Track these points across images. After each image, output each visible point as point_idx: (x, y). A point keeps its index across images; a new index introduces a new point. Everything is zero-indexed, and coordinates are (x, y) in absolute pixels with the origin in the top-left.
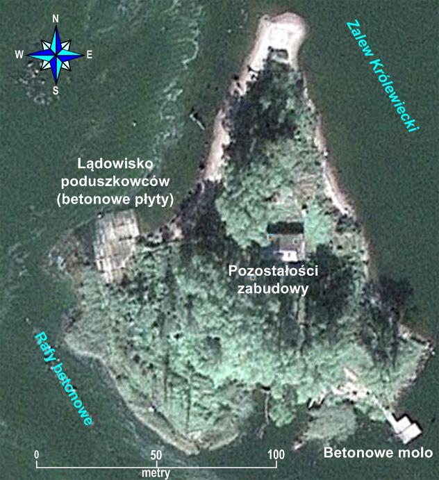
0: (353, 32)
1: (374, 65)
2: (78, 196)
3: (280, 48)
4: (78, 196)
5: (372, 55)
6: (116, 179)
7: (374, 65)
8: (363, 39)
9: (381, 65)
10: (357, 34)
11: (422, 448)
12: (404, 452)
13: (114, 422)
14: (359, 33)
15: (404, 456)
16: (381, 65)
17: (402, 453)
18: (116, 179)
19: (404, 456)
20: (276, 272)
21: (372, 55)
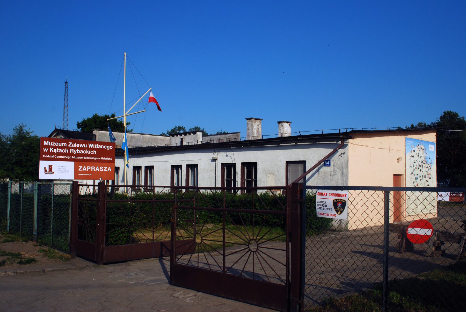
0: (73, 146)
1: (51, 151)
2: (56, 149)
3: (349, 155)
4: (56, 149)
5: (47, 149)
6: (88, 151)
7: (51, 151)
8: (76, 144)
9: (53, 148)
10: (74, 145)
11: (76, 143)
12: (64, 144)
13: (306, 203)
14: (74, 144)
15: (64, 146)
16: (53, 148)
17: (63, 144)
18: (88, 151)
19: (64, 146)
20: (59, 150)
21: (47, 149)
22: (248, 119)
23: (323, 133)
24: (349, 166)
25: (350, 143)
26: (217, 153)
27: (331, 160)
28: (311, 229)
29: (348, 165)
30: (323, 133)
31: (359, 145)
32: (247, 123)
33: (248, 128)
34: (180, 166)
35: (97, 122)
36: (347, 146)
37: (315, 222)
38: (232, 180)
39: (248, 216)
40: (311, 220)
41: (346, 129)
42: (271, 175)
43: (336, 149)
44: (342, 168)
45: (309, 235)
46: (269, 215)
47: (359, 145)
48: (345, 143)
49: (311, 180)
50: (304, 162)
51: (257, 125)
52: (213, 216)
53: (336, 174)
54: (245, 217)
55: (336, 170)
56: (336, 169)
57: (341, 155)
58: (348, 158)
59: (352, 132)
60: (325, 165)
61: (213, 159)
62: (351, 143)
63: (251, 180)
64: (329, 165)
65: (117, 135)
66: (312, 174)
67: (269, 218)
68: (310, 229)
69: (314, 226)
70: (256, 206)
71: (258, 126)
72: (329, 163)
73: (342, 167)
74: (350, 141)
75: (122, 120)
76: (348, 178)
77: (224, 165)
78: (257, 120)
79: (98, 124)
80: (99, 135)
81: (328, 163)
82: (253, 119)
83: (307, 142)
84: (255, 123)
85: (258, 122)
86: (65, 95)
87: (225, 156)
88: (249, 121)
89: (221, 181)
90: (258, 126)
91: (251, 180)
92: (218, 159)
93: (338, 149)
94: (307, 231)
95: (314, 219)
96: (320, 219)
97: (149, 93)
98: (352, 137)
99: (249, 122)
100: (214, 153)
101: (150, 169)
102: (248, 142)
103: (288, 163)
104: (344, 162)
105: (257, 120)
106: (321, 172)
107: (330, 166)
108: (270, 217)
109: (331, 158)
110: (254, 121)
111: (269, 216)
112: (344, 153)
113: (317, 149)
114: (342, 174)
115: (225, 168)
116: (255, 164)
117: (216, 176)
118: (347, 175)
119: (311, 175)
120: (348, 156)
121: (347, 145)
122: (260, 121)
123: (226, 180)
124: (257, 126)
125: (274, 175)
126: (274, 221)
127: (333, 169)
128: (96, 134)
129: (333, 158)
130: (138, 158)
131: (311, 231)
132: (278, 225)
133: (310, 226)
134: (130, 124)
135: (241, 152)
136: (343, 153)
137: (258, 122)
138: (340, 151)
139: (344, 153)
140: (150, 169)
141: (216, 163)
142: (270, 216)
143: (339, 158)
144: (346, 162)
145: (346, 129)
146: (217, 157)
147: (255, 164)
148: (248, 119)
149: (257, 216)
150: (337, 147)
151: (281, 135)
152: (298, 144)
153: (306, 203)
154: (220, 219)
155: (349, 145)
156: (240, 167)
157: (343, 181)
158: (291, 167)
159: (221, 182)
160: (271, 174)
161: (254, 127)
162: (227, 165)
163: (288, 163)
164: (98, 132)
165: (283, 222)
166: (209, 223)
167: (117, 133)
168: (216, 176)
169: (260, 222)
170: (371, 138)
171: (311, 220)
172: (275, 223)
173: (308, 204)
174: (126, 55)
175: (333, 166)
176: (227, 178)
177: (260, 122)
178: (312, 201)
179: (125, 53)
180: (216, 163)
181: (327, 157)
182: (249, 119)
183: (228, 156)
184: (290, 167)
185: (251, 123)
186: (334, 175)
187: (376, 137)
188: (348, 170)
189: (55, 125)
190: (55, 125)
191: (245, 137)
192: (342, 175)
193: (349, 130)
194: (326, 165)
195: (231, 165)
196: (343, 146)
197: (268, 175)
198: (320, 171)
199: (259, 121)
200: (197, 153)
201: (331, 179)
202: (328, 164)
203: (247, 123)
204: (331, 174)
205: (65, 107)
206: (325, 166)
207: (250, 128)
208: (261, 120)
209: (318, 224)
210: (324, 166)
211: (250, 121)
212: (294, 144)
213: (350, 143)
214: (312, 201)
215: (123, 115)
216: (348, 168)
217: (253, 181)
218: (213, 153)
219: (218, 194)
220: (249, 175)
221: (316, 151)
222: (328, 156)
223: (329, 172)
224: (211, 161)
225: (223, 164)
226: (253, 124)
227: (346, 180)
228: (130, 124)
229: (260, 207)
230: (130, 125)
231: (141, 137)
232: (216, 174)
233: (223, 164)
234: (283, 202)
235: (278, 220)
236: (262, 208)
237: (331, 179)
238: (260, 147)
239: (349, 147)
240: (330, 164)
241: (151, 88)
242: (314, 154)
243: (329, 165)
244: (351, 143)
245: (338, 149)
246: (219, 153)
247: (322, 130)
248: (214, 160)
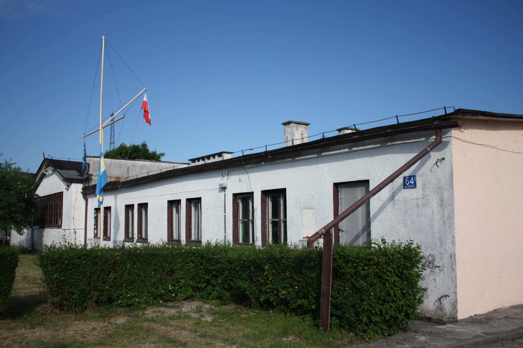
3: (453, 162)
22: (285, 124)
23: (400, 122)
24: (454, 185)
25: (455, 137)
26: (226, 178)
27: (417, 175)
28: (372, 325)
29: (452, 182)
30: (398, 122)
31: (474, 143)
32: (285, 130)
33: (286, 138)
34: (179, 201)
35: (123, 154)
36: (448, 144)
37: (381, 311)
38: (250, 222)
39: (254, 291)
40: (371, 306)
41: (445, 108)
42: (309, 210)
43: (426, 149)
44: (440, 190)
45: (367, 339)
46: (289, 290)
47: (474, 143)
48: (443, 138)
49: (380, 217)
50: (367, 182)
51: (300, 133)
52: (203, 286)
53: (428, 203)
54: (247, 292)
55: (428, 195)
56: (427, 193)
57: (436, 163)
58: (452, 169)
59: (458, 112)
60: (406, 187)
61: (221, 187)
62: (458, 139)
63: (278, 220)
64: (414, 186)
65: (120, 164)
66: (382, 206)
67: (289, 296)
68: (370, 325)
69: (378, 319)
70: (265, 271)
71: (302, 134)
72: (413, 182)
73: (440, 188)
74: (455, 133)
75: (155, 151)
76: (453, 211)
77: (238, 197)
78: (301, 126)
79: (124, 155)
80: (94, 164)
81: (411, 182)
82: (292, 123)
83: (369, 145)
84: (297, 129)
85: (302, 128)
86: (111, 130)
87: (238, 181)
88: (287, 126)
89: (232, 223)
90: (302, 134)
91: (278, 220)
92: (228, 187)
93: (429, 149)
94: (363, 328)
95: (378, 302)
96: (392, 302)
97: (142, 95)
98: (459, 123)
99: (288, 128)
100: (222, 178)
101: (143, 206)
102: (269, 153)
103: (337, 186)
104: (445, 177)
105: (300, 125)
106: (398, 200)
107: (415, 187)
108: (291, 294)
109: (418, 171)
110: (294, 126)
111: (289, 292)
112: (443, 159)
113: (389, 155)
114: (440, 203)
115: (240, 201)
116: (282, 192)
117: (225, 216)
118: (452, 205)
119: (379, 208)
120: (452, 164)
121: (448, 143)
122: (306, 126)
123: (241, 223)
124: (300, 134)
125: (314, 210)
126: (299, 302)
127: (421, 193)
128: (90, 163)
129: (420, 171)
130: (131, 193)
131: (372, 329)
132: (306, 312)
133: (369, 317)
134: (164, 155)
135: (260, 173)
136: (440, 158)
137: (302, 128)
138: (435, 155)
139: (443, 159)
140: (143, 206)
141: (225, 194)
142: (291, 293)
143: (433, 170)
144: (448, 177)
145: (445, 108)
146: (226, 183)
147: (282, 192)
148: (285, 124)
149: (268, 290)
150: (428, 146)
151: (323, 136)
152: (354, 149)
153: (360, 266)
154: (416, 249)
155: (454, 141)
156: (260, 198)
157: (444, 216)
158: (343, 193)
159: (232, 225)
160: (308, 209)
161: (295, 135)
162: (242, 196)
163: (337, 186)
164: (93, 160)
165: (315, 307)
166: (195, 299)
167: (119, 160)
168: (225, 216)
169: (275, 304)
170: (496, 130)
171: (371, 306)
172: (300, 307)
173: (363, 270)
174: (105, 39)
175: (421, 186)
176: (243, 218)
177: (305, 128)
178: (372, 262)
179: (103, 37)
180: (225, 194)
181: (406, 166)
182: (286, 124)
183: (242, 181)
184: (341, 194)
185: (290, 129)
186: (424, 205)
187: (507, 130)
188: (452, 194)
189: (44, 153)
190: (44, 153)
191: (266, 146)
192: (442, 203)
193: (450, 111)
194: (407, 186)
195: (247, 195)
196: (438, 145)
197: (304, 211)
198: (396, 198)
199: (304, 126)
200: (200, 179)
201: (418, 214)
202: (410, 184)
203: (285, 130)
204: (417, 205)
205: (111, 143)
206: (406, 188)
207: (288, 138)
208: (307, 125)
209: (387, 314)
210: (404, 188)
211: (288, 127)
212: (347, 150)
213: (455, 137)
214: (372, 262)
215: (99, 127)
216: (453, 189)
217: (281, 222)
218: (221, 178)
219: (161, 248)
220: (276, 213)
221: (388, 159)
222: (408, 165)
223: (414, 200)
224: (219, 190)
225: (235, 195)
226: (294, 132)
227: (449, 215)
228: (164, 155)
229: (273, 273)
230: (165, 156)
231: (156, 166)
232: (225, 213)
233: (235, 195)
234: (314, 263)
235: (304, 302)
236: (276, 274)
237: (418, 214)
238: (290, 162)
239: (452, 147)
240: (415, 183)
241: (146, 88)
242: (384, 166)
243: (414, 186)
244: (458, 139)
245: (429, 149)
246: (229, 177)
247: (397, 117)
248: (223, 189)
